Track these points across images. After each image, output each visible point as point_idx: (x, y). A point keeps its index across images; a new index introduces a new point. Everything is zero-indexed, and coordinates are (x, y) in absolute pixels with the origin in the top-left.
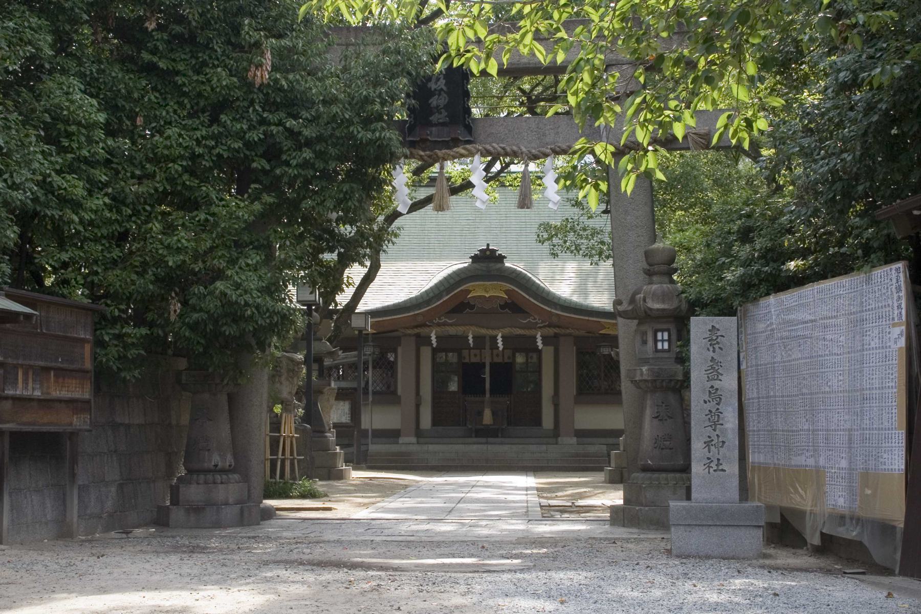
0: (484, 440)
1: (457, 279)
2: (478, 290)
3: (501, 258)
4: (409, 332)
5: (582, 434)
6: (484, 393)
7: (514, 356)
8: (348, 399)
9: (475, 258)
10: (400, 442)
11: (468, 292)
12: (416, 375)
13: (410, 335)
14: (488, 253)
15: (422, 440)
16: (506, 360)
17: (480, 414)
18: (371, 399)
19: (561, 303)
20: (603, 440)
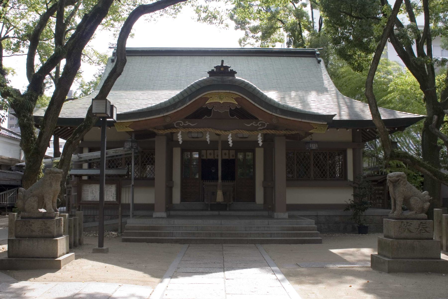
0: (216, 213)
1: (198, 87)
2: (216, 98)
3: (233, 73)
4: (161, 132)
5: (291, 208)
6: (217, 179)
7: (236, 155)
8: (114, 184)
9: (211, 73)
10: (154, 216)
11: (207, 99)
12: (170, 169)
13: (161, 135)
14: (222, 69)
15: (172, 213)
16: (231, 158)
17: (214, 194)
18: (133, 183)
19: (280, 107)
20: (314, 213)
